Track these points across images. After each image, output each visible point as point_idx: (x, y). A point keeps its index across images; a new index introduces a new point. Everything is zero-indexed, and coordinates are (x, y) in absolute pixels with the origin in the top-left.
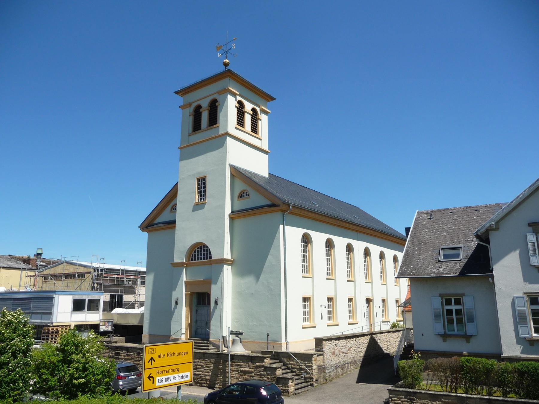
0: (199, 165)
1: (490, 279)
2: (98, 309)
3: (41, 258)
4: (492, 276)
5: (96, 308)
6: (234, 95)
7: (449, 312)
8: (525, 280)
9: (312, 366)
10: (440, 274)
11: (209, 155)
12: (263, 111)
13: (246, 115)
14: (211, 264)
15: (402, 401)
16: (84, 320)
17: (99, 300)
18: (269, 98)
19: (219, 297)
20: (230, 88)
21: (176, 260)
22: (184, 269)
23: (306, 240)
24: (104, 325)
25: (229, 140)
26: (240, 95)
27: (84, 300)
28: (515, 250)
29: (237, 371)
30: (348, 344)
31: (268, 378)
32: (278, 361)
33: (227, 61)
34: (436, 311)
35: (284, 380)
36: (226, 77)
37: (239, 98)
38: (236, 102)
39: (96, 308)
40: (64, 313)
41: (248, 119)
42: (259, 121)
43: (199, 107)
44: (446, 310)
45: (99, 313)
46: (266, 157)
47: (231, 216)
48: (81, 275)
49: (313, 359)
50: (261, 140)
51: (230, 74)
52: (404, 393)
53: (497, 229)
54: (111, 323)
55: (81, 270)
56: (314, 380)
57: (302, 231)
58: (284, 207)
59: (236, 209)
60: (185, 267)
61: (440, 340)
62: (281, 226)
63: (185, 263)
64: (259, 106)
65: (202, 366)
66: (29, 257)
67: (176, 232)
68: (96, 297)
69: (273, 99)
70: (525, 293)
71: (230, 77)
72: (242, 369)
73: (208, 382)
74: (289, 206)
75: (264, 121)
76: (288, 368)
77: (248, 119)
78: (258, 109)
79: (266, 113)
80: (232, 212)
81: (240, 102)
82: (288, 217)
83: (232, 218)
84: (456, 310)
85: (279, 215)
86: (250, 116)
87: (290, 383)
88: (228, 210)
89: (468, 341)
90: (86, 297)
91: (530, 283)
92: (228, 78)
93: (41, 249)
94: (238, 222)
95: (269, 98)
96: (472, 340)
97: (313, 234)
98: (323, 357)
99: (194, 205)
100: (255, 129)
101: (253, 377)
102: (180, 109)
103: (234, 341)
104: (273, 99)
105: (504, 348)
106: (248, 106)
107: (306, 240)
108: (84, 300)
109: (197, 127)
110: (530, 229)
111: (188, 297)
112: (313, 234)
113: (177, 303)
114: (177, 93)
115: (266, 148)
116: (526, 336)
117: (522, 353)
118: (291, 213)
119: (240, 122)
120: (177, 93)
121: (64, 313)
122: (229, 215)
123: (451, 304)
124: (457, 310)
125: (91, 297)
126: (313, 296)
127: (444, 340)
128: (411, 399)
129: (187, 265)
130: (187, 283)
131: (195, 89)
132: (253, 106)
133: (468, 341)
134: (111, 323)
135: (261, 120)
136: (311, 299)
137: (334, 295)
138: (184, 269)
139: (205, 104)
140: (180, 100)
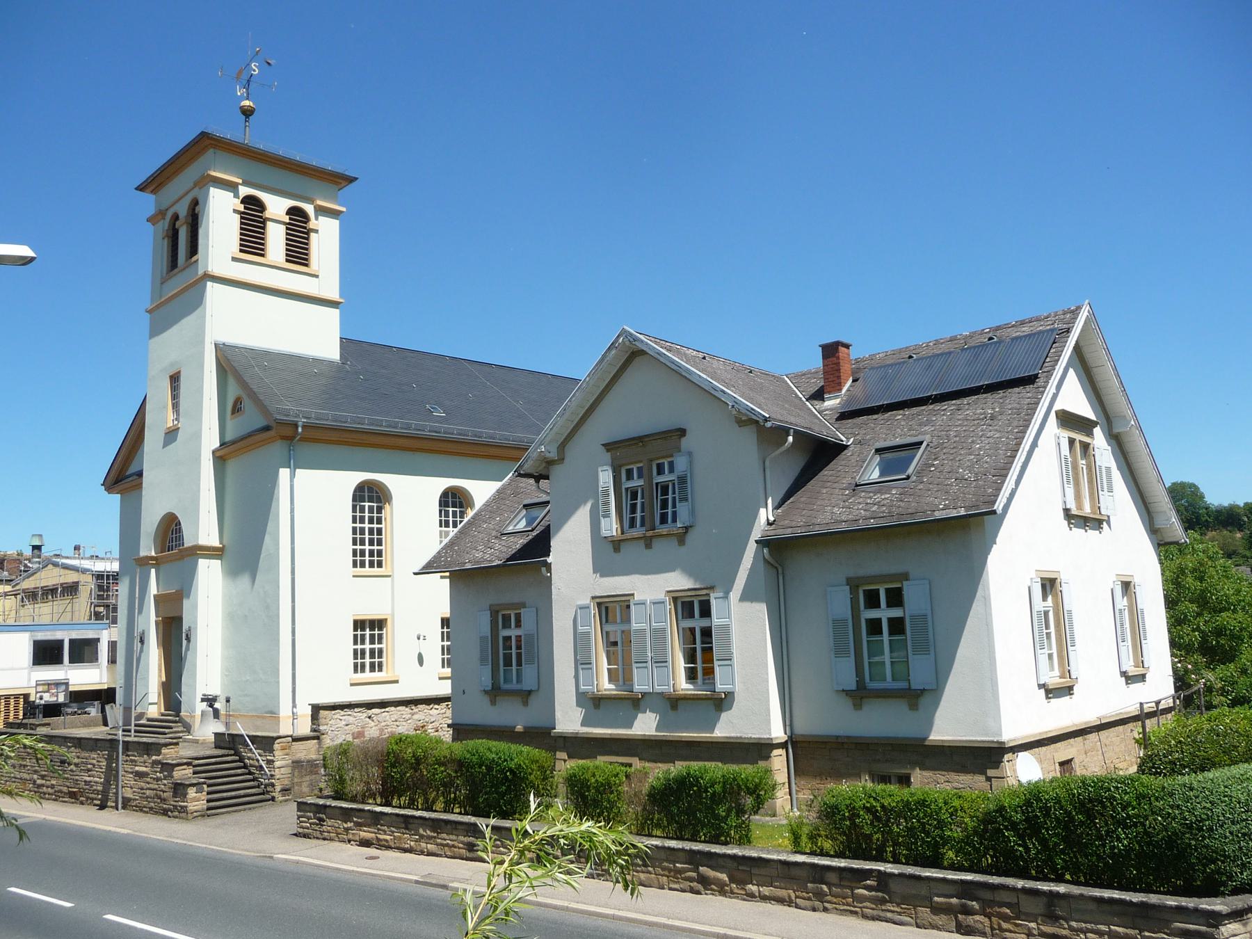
0: (167, 348)
1: (544, 569)
3: (39, 557)
4: (548, 566)
5: (94, 658)
6: (231, 187)
7: (874, 627)
10: (478, 562)
11: (185, 321)
12: (321, 211)
13: (270, 226)
18: (339, 180)
22: (153, 571)
23: (371, 497)
26: (245, 183)
27: (61, 642)
30: (416, 717)
33: (247, 103)
34: (838, 624)
36: (204, 150)
37: (244, 191)
38: (238, 201)
39: (94, 658)
40: (12, 669)
41: (276, 237)
42: (313, 235)
43: (176, 217)
44: (867, 620)
45: (98, 667)
47: (218, 454)
48: (71, 589)
49: (276, 746)
50: (317, 276)
53: (561, 460)
54: (63, 687)
55: (71, 577)
56: (278, 788)
59: (229, 438)
60: (153, 566)
62: (284, 473)
63: (152, 558)
64: (310, 200)
66: (20, 554)
68: (90, 635)
69: (351, 180)
70: (593, 598)
74: (296, 426)
75: (326, 236)
76: (245, 767)
77: (276, 237)
78: (309, 209)
81: (250, 201)
83: (220, 459)
84: (891, 620)
85: (278, 448)
86: (282, 228)
88: (210, 439)
91: (601, 576)
93: (41, 536)
94: (232, 466)
95: (339, 180)
96: (533, 700)
97: (391, 481)
98: (320, 744)
100: (298, 253)
103: (203, 713)
104: (351, 180)
106: (277, 206)
107: (371, 497)
108: (61, 642)
109: (173, 263)
111: (161, 627)
112: (391, 481)
113: (142, 641)
114: (141, 188)
115: (334, 295)
118: (303, 439)
120: (141, 188)
121: (12, 669)
123: (878, 606)
124: (891, 621)
125: (76, 635)
126: (393, 615)
129: (157, 562)
133: (526, 703)
134: (63, 687)
135: (316, 231)
136: (389, 622)
138: (153, 571)
139: (182, 209)
140: (148, 203)
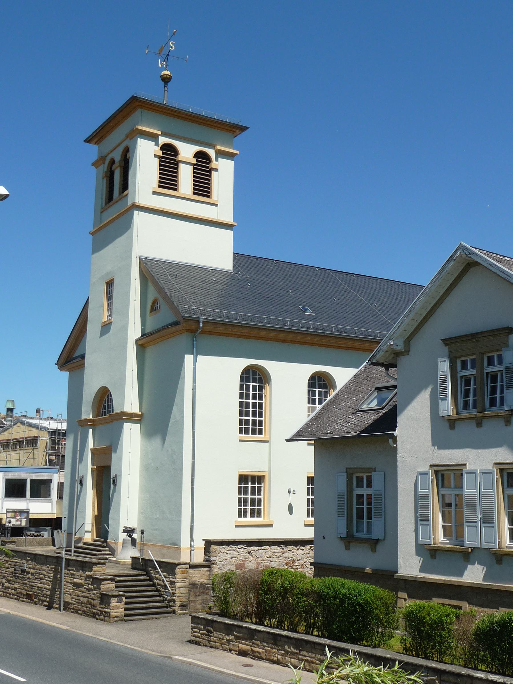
0: (105, 262)
1: (391, 441)
2: (49, 496)
5: (47, 495)
6: (153, 137)
8: (433, 445)
9: (175, 582)
12: (220, 154)
13: (182, 166)
14: (112, 421)
15: (201, 634)
16: (49, 511)
17: (51, 481)
19: (118, 475)
20: (140, 128)
21: (84, 417)
22: (91, 431)
23: (254, 379)
24: (14, 517)
25: (138, 216)
26: (164, 134)
27: (25, 481)
28: (426, 387)
29: (71, 583)
30: (286, 555)
31: (94, 594)
32: (145, 573)
33: (166, 72)
35: (106, 597)
37: (163, 140)
39: (47, 495)
41: (186, 175)
42: (214, 173)
45: (50, 501)
46: (229, 234)
47: (140, 342)
49: (177, 571)
50: (216, 205)
51: (138, 103)
52: (203, 621)
53: (407, 352)
54: (25, 515)
56: (178, 604)
57: (239, 364)
58: (192, 326)
59: (147, 331)
60: (91, 427)
61: (341, 545)
62: (188, 358)
63: (90, 421)
64: (211, 146)
65: (44, 575)
67: (85, 371)
68: (45, 476)
69: (244, 129)
71: (141, 107)
72: (75, 580)
73: (48, 599)
74: (198, 322)
75: (224, 174)
77: (186, 175)
78: (211, 152)
79: (230, 156)
80: (144, 335)
82: (205, 341)
83: (142, 346)
85: (184, 339)
87: (114, 602)
88: (135, 332)
89: (374, 550)
90: (28, 476)
91: (439, 448)
92: (139, 110)
93: (13, 401)
95: (234, 129)
97: (272, 367)
99: (102, 326)
100: (202, 188)
101: (83, 592)
102: (94, 167)
104: (244, 129)
105: (401, 561)
106: (187, 151)
107: (254, 379)
108: (25, 481)
110: (446, 349)
111: (95, 473)
113: (81, 484)
115: (229, 219)
116: (490, 545)
117: (484, 579)
118: (203, 332)
119: (168, 179)
122: (137, 341)
126: (270, 473)
127: (347, 548)
128: (209, 632)
130: (94, 452)
131: (109, 132)
132: (197, 148)
133: (374, 550)
134: (25, 515)
135: (216, 170)
137: (267, 470)
138: (91, 431)
139: (117, 156)
